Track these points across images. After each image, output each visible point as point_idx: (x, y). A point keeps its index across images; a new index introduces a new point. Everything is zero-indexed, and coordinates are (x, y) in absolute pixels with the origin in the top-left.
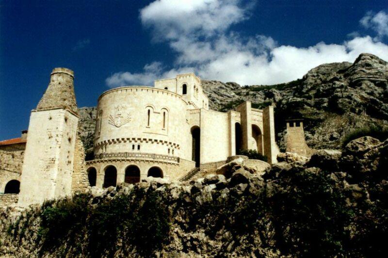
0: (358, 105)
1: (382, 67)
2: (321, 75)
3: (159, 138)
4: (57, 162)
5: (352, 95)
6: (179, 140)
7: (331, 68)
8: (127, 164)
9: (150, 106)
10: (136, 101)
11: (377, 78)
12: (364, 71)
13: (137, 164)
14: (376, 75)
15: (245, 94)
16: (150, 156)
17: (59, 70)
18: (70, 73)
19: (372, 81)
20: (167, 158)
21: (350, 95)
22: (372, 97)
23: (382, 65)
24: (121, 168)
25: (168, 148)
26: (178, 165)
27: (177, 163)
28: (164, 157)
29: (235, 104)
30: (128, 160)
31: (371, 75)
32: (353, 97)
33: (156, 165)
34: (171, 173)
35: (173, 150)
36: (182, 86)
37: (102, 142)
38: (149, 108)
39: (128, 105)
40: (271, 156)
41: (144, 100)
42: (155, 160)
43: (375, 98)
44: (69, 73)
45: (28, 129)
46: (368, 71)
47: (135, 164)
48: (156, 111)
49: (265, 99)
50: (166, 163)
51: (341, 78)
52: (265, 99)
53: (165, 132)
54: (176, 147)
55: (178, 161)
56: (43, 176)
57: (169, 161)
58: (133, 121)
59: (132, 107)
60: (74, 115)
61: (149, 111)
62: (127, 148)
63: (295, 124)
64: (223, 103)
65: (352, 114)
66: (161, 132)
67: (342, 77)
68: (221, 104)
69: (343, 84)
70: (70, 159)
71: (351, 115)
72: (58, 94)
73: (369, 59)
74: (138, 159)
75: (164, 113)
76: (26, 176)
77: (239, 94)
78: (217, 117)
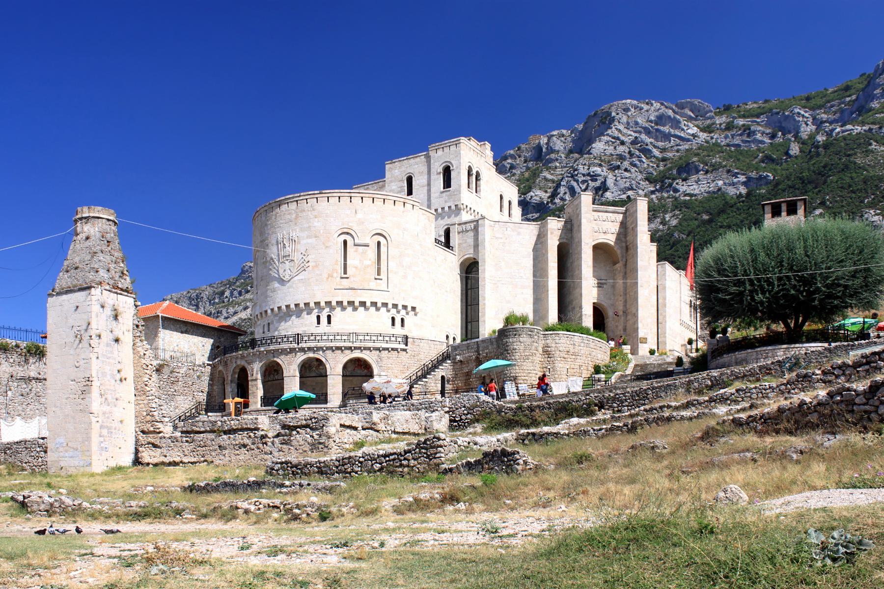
3: (368, 298)
4: (96, 384)
8: (301, 357)
9: (348, 233)
10: (316, 224)
13: (319, 355)
15: (723, 126)
16: (345, 337)
18: (107, 214)
24: (290, 364)
25: (390, 315)
26: (405, 350)
29: (697, 155)
30: (302, 350)
33: (357, 354)
34: (388, 368)
35: (402, 320)
36: (441, 170)
37: (288, 306)
40: (637, 310)
41: (332, 219)
44: (101, 216)
45: (46, 327)
47: (316, 356)
49: (773, 136)
50: (378, 349)
52: (773, 136)
53: (382, 285)
54: (407, 313)
57: (385, 345)
59: (309, 237)
61: (345, 242)
63: (784, 207)
64: (670, 155)
66: (373, 284)
68: (664, 160)
70: (123, 374)
75: (379, 243)
76: (54, 409)
77: (708, 129)
78: (519, 234)
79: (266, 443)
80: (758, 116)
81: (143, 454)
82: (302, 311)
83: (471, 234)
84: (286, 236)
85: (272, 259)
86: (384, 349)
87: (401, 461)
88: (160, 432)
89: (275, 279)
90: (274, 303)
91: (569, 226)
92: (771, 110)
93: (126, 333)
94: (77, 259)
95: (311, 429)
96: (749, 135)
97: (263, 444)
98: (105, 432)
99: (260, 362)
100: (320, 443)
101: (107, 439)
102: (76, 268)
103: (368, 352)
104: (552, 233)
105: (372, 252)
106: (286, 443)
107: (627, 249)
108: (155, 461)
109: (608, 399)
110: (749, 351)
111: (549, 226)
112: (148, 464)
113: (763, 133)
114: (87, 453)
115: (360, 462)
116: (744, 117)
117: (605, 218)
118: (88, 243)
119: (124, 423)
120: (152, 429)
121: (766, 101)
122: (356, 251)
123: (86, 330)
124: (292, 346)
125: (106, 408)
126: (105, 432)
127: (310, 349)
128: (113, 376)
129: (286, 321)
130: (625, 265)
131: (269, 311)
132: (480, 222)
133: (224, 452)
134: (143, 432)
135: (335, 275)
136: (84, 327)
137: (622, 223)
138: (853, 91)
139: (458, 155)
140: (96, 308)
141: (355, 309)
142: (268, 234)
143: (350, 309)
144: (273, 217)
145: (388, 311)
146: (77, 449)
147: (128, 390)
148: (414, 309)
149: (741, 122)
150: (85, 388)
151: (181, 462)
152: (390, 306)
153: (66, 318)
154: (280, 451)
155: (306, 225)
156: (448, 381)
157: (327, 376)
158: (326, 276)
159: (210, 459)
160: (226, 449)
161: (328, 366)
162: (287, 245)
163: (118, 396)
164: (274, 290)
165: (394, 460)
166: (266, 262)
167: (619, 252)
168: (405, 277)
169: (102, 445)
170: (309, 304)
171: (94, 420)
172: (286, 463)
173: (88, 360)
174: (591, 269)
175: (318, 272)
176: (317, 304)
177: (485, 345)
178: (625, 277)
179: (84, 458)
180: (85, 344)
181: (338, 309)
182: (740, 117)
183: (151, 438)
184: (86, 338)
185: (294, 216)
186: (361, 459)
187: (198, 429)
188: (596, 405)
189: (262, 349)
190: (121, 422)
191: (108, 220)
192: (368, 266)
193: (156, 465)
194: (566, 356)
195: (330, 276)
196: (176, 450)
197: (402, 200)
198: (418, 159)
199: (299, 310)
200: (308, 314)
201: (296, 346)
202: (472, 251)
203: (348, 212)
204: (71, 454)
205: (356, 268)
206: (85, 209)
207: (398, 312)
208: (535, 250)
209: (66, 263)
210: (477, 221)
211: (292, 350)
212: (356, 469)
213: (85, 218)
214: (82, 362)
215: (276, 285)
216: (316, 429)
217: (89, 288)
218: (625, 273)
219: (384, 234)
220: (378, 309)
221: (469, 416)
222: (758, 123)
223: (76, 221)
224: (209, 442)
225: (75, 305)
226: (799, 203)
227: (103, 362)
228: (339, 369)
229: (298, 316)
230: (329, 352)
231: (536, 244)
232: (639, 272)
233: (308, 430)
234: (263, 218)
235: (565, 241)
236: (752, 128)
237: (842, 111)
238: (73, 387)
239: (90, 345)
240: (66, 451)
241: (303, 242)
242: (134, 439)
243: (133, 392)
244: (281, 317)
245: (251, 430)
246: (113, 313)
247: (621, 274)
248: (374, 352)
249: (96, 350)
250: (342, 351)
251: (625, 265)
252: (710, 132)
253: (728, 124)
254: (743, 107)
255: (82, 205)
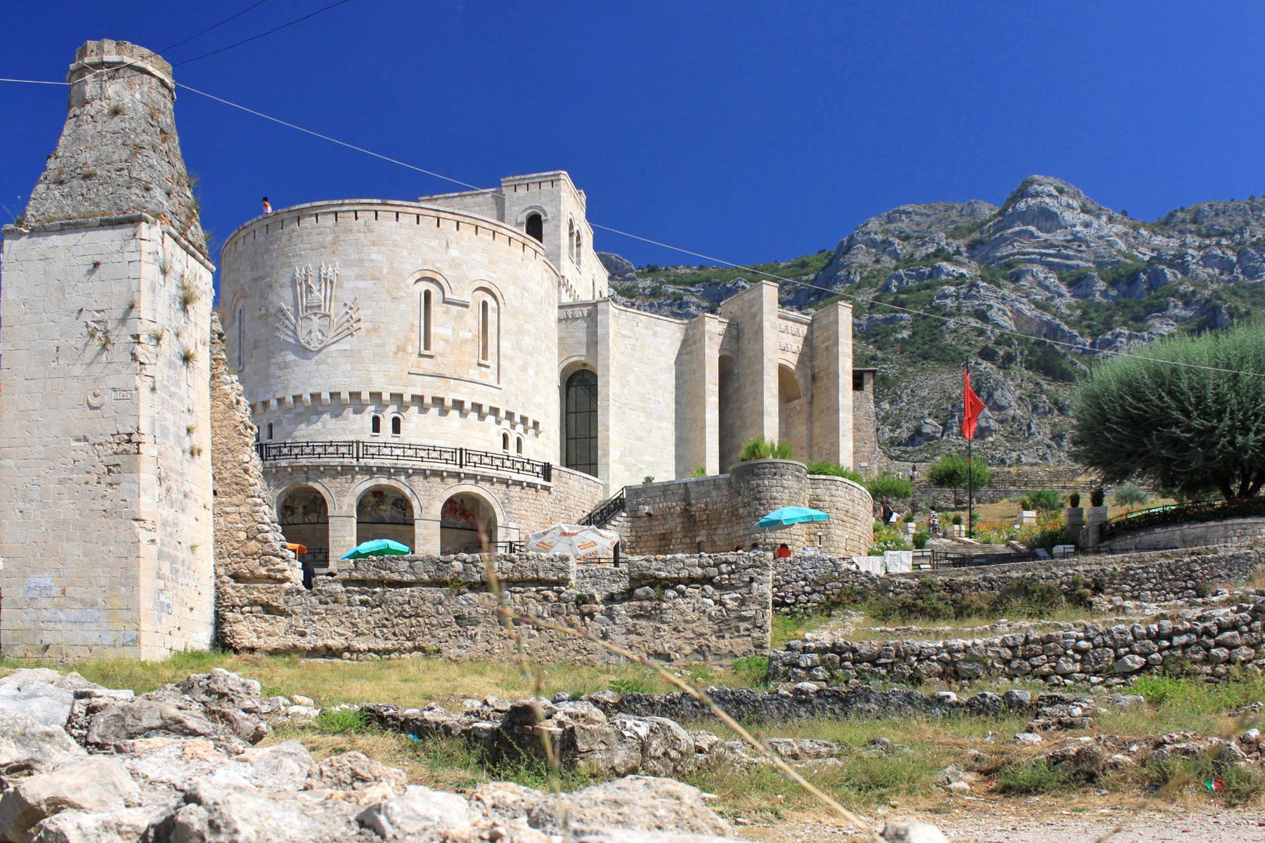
0: (1003, 340)
1: (1087, 225)
2: (897, 241)
3: (468, 396)
4: (148, 450)
5: (991, 307)
6: (538, 406)
7: (929, 220)
8: (363, 484)
9: (432, 280)
10: (374, 256)
11: (1068, 257)
12: (1032, 235)
13: (400, 483)
14: (1066, 248)
15: (647, 292)
17: (110, 52)
18: (159, 68)
19: (1051, 266)
20: (487, 460)
21: (984, 308)
22: (1048, 317)
23: (1087, 217)
24: (341, 493)
26: (547, 489)
27: (540, 481)
28: (518, 466)
30: (367, 470)
31: (1052, 246)
32: (993, 314)
33: (468, 487)
35: (519, 440)
38: (425, 286)
39: (346, 272)
41: (405, 252)
42: (466, 470)
43: (1058, 321)
44: (150, 68)
46: (1044, 236)
47: (393, 483)
48: (455, 297)
50: (505, 482)
51: (958, 252)
54: (526, 431)
55: (548, 478)
56: (98, 505)
57: (516, 477)
58: (368, 331)
60: (193, 256)
61: (427, 295)
62: (356, 426)
65: (985, 365)
66: (475, 373)
67: (963, 249)
69: (964, 271)
71: (981, 368)
72: (115, 157)
73: (1050, 195)
74: (400, 463)
76: (21, 505)
78: (655, 334)
79: (591, 616)
80: (692, 284)
81: (237, 627)
82: (344, 406)
83: (582, 325)
84: (315, 273)
85: (281, 310)
86: (516, 483)
87: (1208, 649)
88: (282, 581)
89: (287, 346)
90: (286, 388)
91: (734, 332)
92: (708, 280)
93: (200, 347)
94: (88, 157)
95: (719, 586)
96: (680, 306)
97: (583, 615)
98: (166, 567)
99: (278, 487)
100: (743, 619)
101: (170, 584)
102: (87, 177)
103: (488, 485)
104: (711, 339)
105: (472, 319)
106: (648, 617)
107: (814, 378)
108: (274, 643)
109: (1113, 576)
110: (1212, 523)
111: (707, 327)
112: (252, 650)
113: (698, 306)
114: (127, 615)
115: (1077, 650)
116: (674, 283)
117: (783, 327)
118: (116, 123)
119: (198, 551)
120: (263, 571)
121: (701, 268)
122: (447, 312)
123: (123, 321)
124: (346, 461)
125: (167, 512)
126: (166, 567)
127: (381, 470)
128: (179, 439)
129: (309, 423)
130: (811, 403)
131: (274, 403)
132: (600, 306)
133: (471, 630)
134: (236, 577)
135: (410, 349)
136: (118, 313)
137: (806, 339)
138: (810, 269)
139: (556, 199)
140: (149, 271)
141: (444, 412)
142: (273, 267)
143: (434, 411)
144: (285, 239)
145: (498, 422)
146: (93, 605)
147: (200, 476)
148: (536, 424)
149: (671, 289)
150: (117, 459)
151: (348, 649)
152: (502, 414)
153: (62, 290)
154: (629, 632)
155: (354, 257)
156: (624, 547)
157: (413, 525)
158: (394, 349)
159: (431, 645)
160: (476, 623)
161: (415, 504)
162: (315, 288)
163: (187, 487)
164: (286, 366)
165: (1185, 646)
166: (267, 315)
167: (801, 382)
168: (524, 369)
169: (162, 598)
170: (359, 394)
171: (144, 536)
172: (834, 648)
173: (128, 395)
174: (777, 400)
175: (378, 341)
176: (376, 396)
177: (702, 489)
178: (810, 420)
179: (120, 626)
180: (118, 353)
181: (414, 410)
182: (669, 282)
183: (259, 592)
184: (121, 338)
185: (330, 238)
186: (1083, 644)
187: (396, 577)
188: (1087, 586)
189: (284, 463)
190: (193, 548)
191: (162, 82)
192: (466, 341)
193: (274, 653)
194: (845, 518)
195: (401, 349)
196: (333, 621)
197: (521, 239)
198: (480, 198)
199: (337, 404)
200: (355, 412)
201: (354, 462)
202: (583, 351)
203: (434, 243)
204: (74, 614)
205: (447, 341)
206: (109, 45)
207: (513, 427)
208: (678, 362)
209: (52, 164)
210: (595, 305)
211: (347, 470)
212: (1068, 666)
213: (110, 65)
214: (108, 397)
215: (291, 357)
216: (732, 587)
217: (134, 221)
218: (811, 414)
219: (494, 290)
220: (482, 417)
221: (815, 596)
222: (692, 293)
223: (83, 70)
224: (428, 607)
225: (90, 260)
226: (866, 376)
227: (163, 402)
228: (436, 510)
229: (337, 415)
230: (418, 481)
231: (680, 354)
232: (841, 414)
233: (709, 588)
234: (261, 239)
235: (728, 353)
236: (685, 298)
237: (798, 291)
238: (81, 456)
239: (134, 357)
240: (60, 607)
241: (348, 285)
242: (213, 590)
243: (210, 485)
244: (300, 414)
245: (550, 584)
246: (181, 293)
247: (804, 416)
248: (497, 486)
249: (149, 370)
250: (443, 478)
251: (811, 403)
252: (630, 297)
253: (654, 289)
254: (673, 270)
255: (98, 37)
